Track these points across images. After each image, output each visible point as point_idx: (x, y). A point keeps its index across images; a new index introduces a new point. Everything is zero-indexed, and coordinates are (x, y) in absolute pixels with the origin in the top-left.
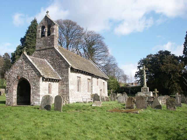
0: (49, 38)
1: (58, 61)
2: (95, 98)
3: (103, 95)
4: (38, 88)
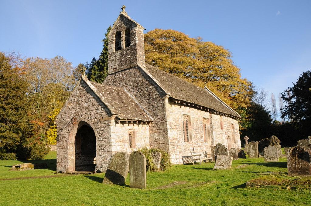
0: (129, 50)
1: (146, 89)
2: (219, 150)
3: (232, 147)
4: (107, 139)
